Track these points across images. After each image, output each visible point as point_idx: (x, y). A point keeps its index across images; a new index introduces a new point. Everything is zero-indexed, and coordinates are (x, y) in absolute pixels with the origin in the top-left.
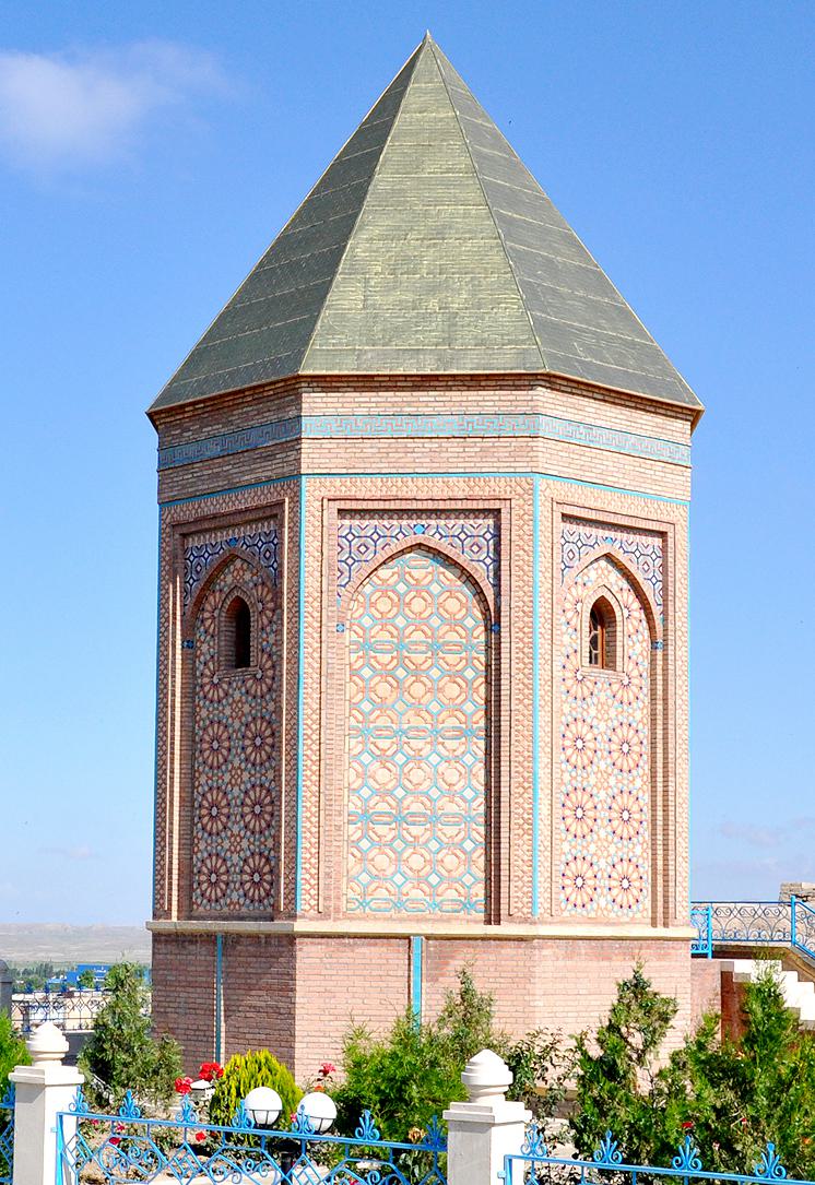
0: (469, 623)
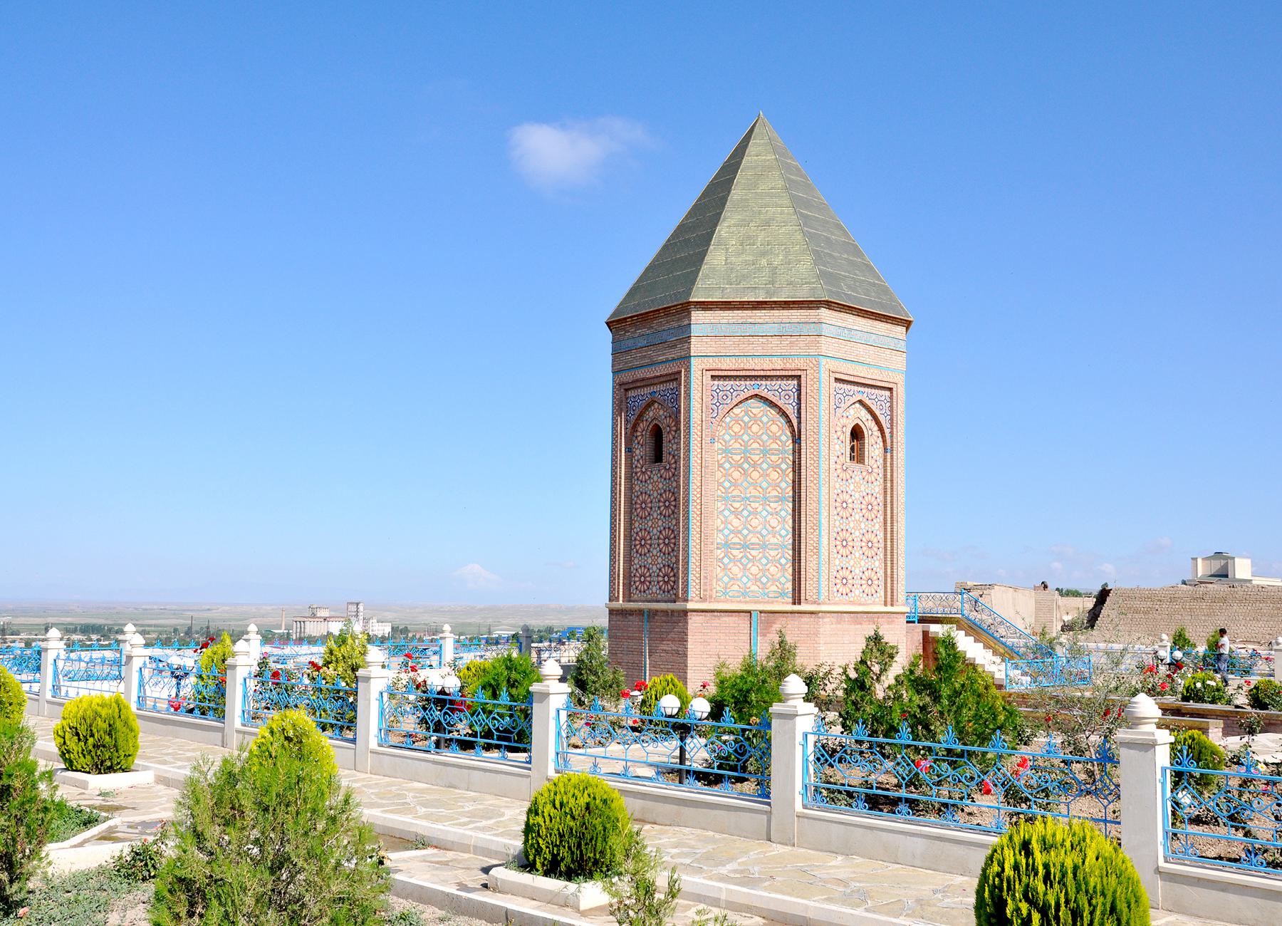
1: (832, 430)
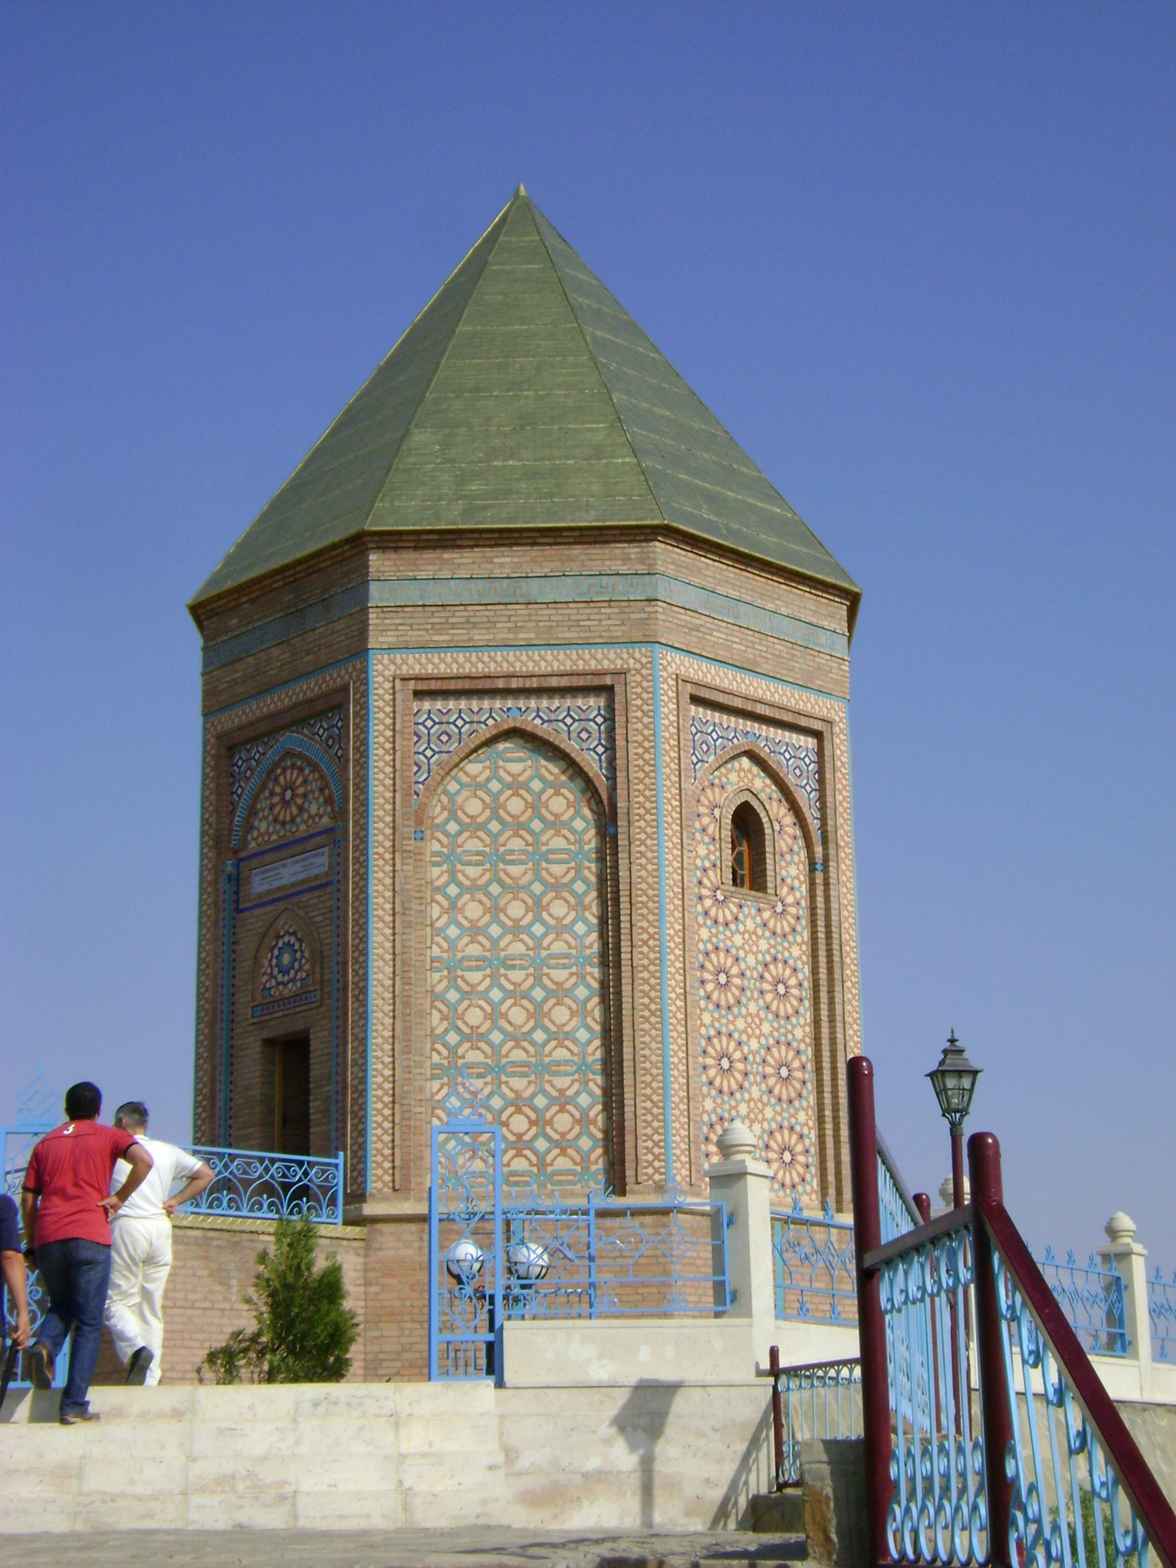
0: (579, 824)
1: (691, 899)
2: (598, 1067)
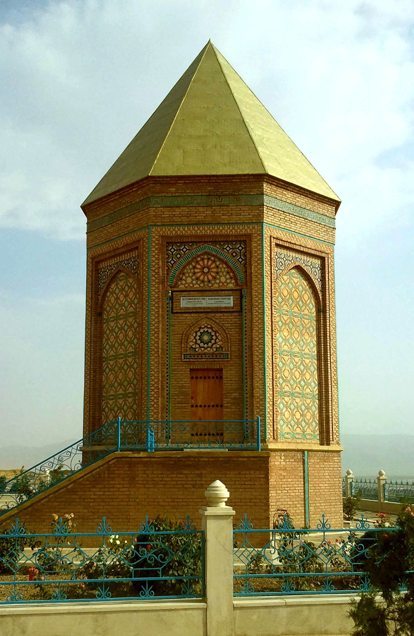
2: (317, 397)
